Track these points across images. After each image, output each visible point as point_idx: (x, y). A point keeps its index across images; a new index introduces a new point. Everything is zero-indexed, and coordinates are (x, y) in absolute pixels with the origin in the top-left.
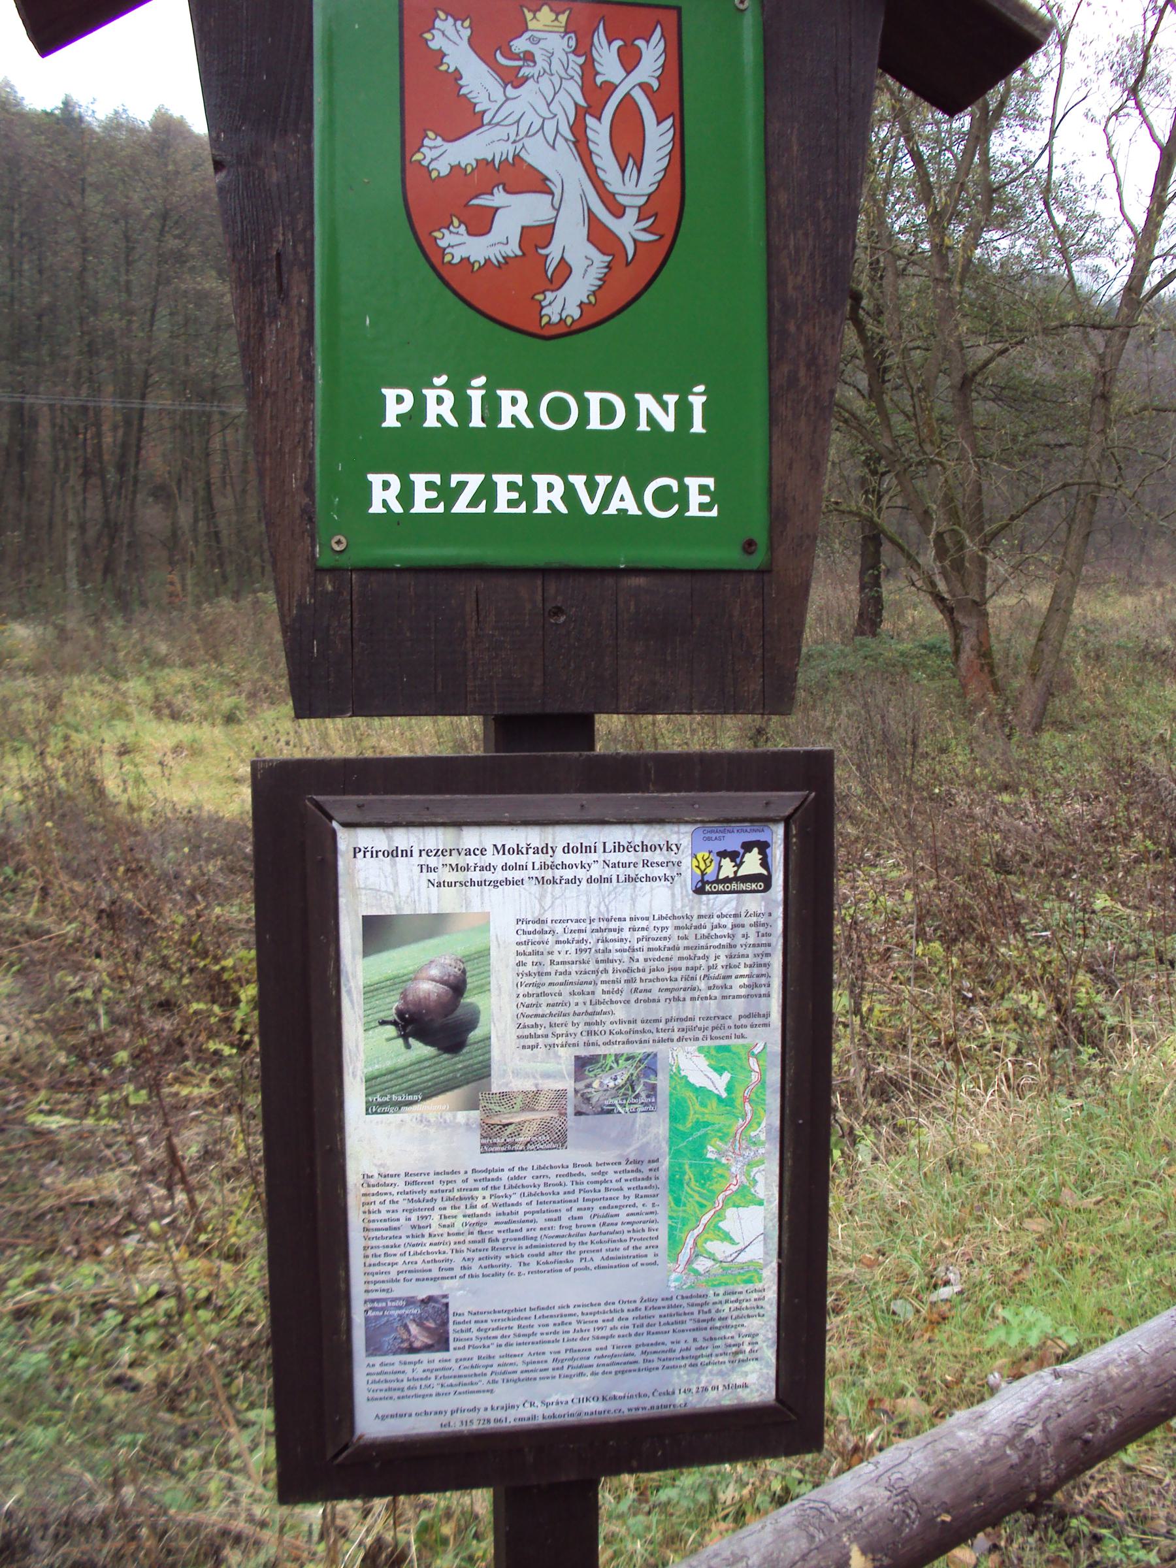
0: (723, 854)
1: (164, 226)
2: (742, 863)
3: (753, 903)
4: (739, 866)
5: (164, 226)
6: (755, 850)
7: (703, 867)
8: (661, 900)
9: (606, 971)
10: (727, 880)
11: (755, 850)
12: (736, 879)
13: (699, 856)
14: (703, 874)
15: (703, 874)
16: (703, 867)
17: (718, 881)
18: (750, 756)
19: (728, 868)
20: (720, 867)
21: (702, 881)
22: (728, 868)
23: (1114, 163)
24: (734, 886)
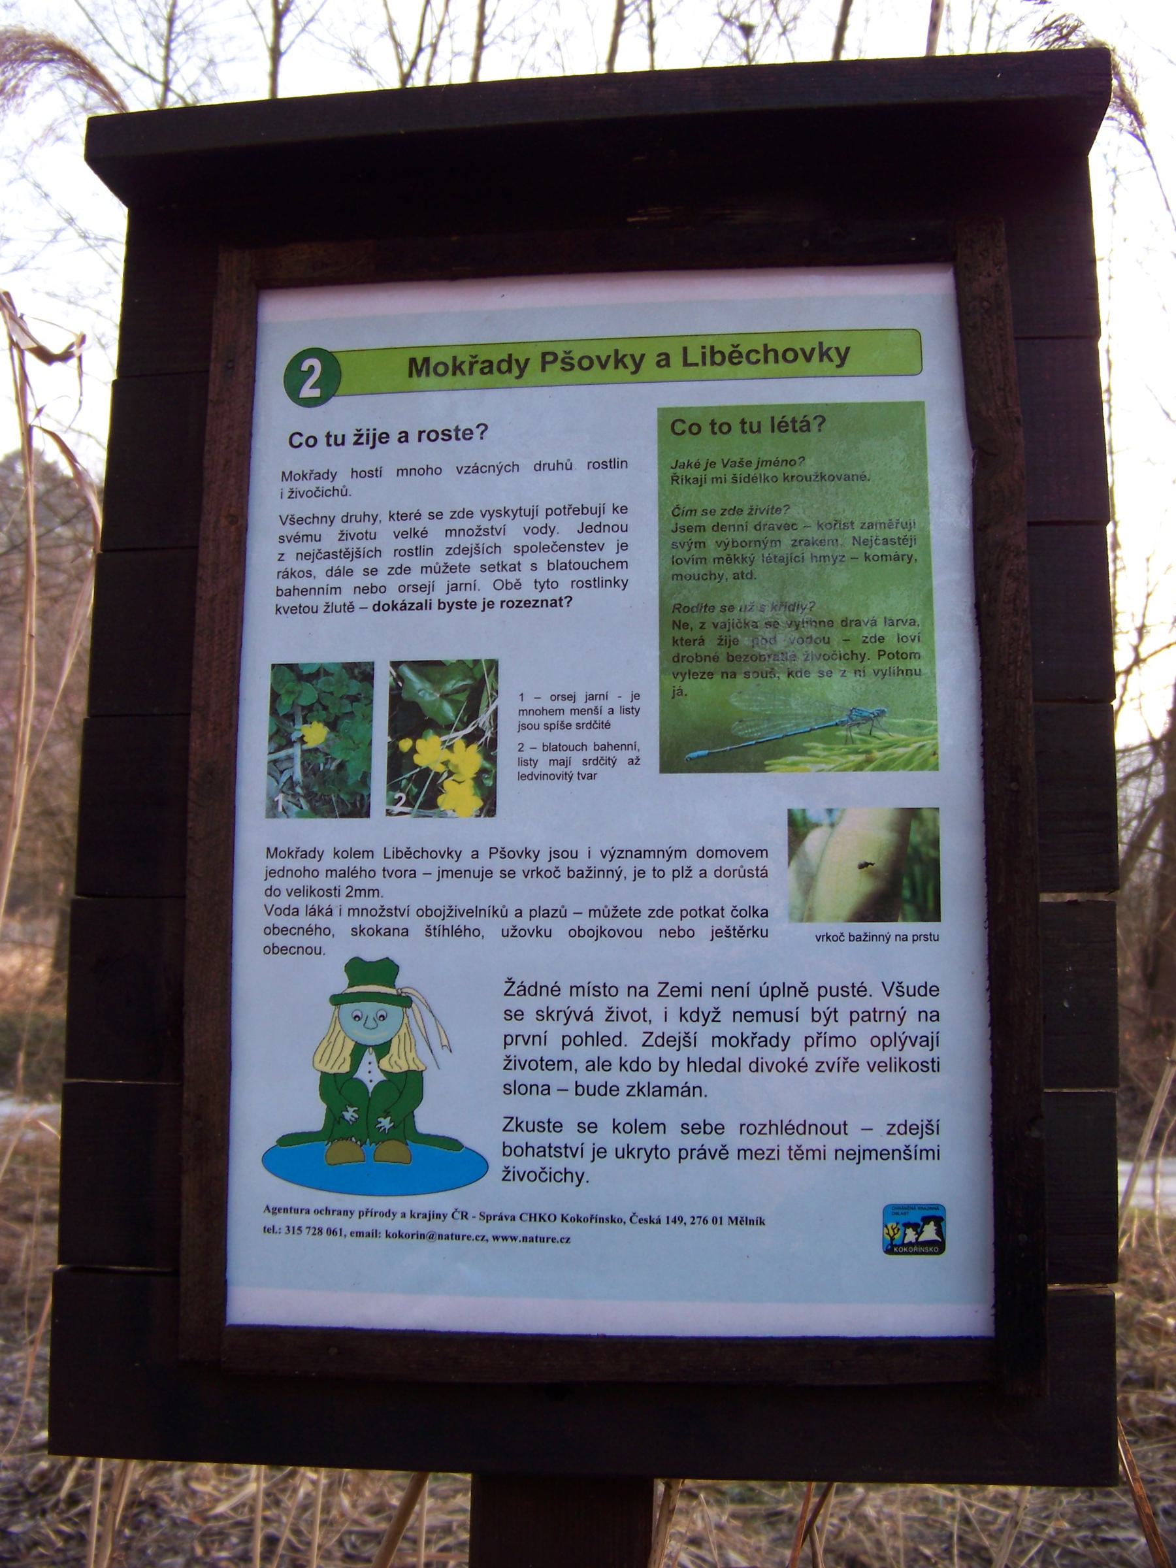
0: (907, 1225)
1: (170, 31)
2: (922, 1232)
3: (323, 642)
4: (919, 1234)
5: (170, 31)
6: (932, 1223)
7: (891, 1233)
8: (1079, 1495)
9: (590, 1015)
10: (910, 1244)
11: (932, 1223)
12: (917, 1243)
13: (889, 1226)
14: (892, 1239)
15: (892, 1239)
16: (891, 1233)
17: (903, 1245)
18: (1113, 1315)
19: (911, 1236)
20: (905, 1235)
21: (891, 1244)
22: (911, 1236)
23: (480, 47)
24: (915, 1249)
